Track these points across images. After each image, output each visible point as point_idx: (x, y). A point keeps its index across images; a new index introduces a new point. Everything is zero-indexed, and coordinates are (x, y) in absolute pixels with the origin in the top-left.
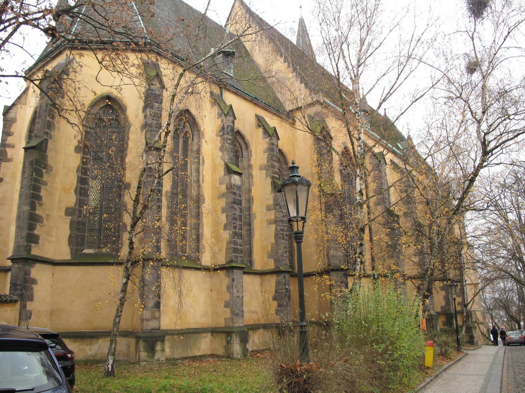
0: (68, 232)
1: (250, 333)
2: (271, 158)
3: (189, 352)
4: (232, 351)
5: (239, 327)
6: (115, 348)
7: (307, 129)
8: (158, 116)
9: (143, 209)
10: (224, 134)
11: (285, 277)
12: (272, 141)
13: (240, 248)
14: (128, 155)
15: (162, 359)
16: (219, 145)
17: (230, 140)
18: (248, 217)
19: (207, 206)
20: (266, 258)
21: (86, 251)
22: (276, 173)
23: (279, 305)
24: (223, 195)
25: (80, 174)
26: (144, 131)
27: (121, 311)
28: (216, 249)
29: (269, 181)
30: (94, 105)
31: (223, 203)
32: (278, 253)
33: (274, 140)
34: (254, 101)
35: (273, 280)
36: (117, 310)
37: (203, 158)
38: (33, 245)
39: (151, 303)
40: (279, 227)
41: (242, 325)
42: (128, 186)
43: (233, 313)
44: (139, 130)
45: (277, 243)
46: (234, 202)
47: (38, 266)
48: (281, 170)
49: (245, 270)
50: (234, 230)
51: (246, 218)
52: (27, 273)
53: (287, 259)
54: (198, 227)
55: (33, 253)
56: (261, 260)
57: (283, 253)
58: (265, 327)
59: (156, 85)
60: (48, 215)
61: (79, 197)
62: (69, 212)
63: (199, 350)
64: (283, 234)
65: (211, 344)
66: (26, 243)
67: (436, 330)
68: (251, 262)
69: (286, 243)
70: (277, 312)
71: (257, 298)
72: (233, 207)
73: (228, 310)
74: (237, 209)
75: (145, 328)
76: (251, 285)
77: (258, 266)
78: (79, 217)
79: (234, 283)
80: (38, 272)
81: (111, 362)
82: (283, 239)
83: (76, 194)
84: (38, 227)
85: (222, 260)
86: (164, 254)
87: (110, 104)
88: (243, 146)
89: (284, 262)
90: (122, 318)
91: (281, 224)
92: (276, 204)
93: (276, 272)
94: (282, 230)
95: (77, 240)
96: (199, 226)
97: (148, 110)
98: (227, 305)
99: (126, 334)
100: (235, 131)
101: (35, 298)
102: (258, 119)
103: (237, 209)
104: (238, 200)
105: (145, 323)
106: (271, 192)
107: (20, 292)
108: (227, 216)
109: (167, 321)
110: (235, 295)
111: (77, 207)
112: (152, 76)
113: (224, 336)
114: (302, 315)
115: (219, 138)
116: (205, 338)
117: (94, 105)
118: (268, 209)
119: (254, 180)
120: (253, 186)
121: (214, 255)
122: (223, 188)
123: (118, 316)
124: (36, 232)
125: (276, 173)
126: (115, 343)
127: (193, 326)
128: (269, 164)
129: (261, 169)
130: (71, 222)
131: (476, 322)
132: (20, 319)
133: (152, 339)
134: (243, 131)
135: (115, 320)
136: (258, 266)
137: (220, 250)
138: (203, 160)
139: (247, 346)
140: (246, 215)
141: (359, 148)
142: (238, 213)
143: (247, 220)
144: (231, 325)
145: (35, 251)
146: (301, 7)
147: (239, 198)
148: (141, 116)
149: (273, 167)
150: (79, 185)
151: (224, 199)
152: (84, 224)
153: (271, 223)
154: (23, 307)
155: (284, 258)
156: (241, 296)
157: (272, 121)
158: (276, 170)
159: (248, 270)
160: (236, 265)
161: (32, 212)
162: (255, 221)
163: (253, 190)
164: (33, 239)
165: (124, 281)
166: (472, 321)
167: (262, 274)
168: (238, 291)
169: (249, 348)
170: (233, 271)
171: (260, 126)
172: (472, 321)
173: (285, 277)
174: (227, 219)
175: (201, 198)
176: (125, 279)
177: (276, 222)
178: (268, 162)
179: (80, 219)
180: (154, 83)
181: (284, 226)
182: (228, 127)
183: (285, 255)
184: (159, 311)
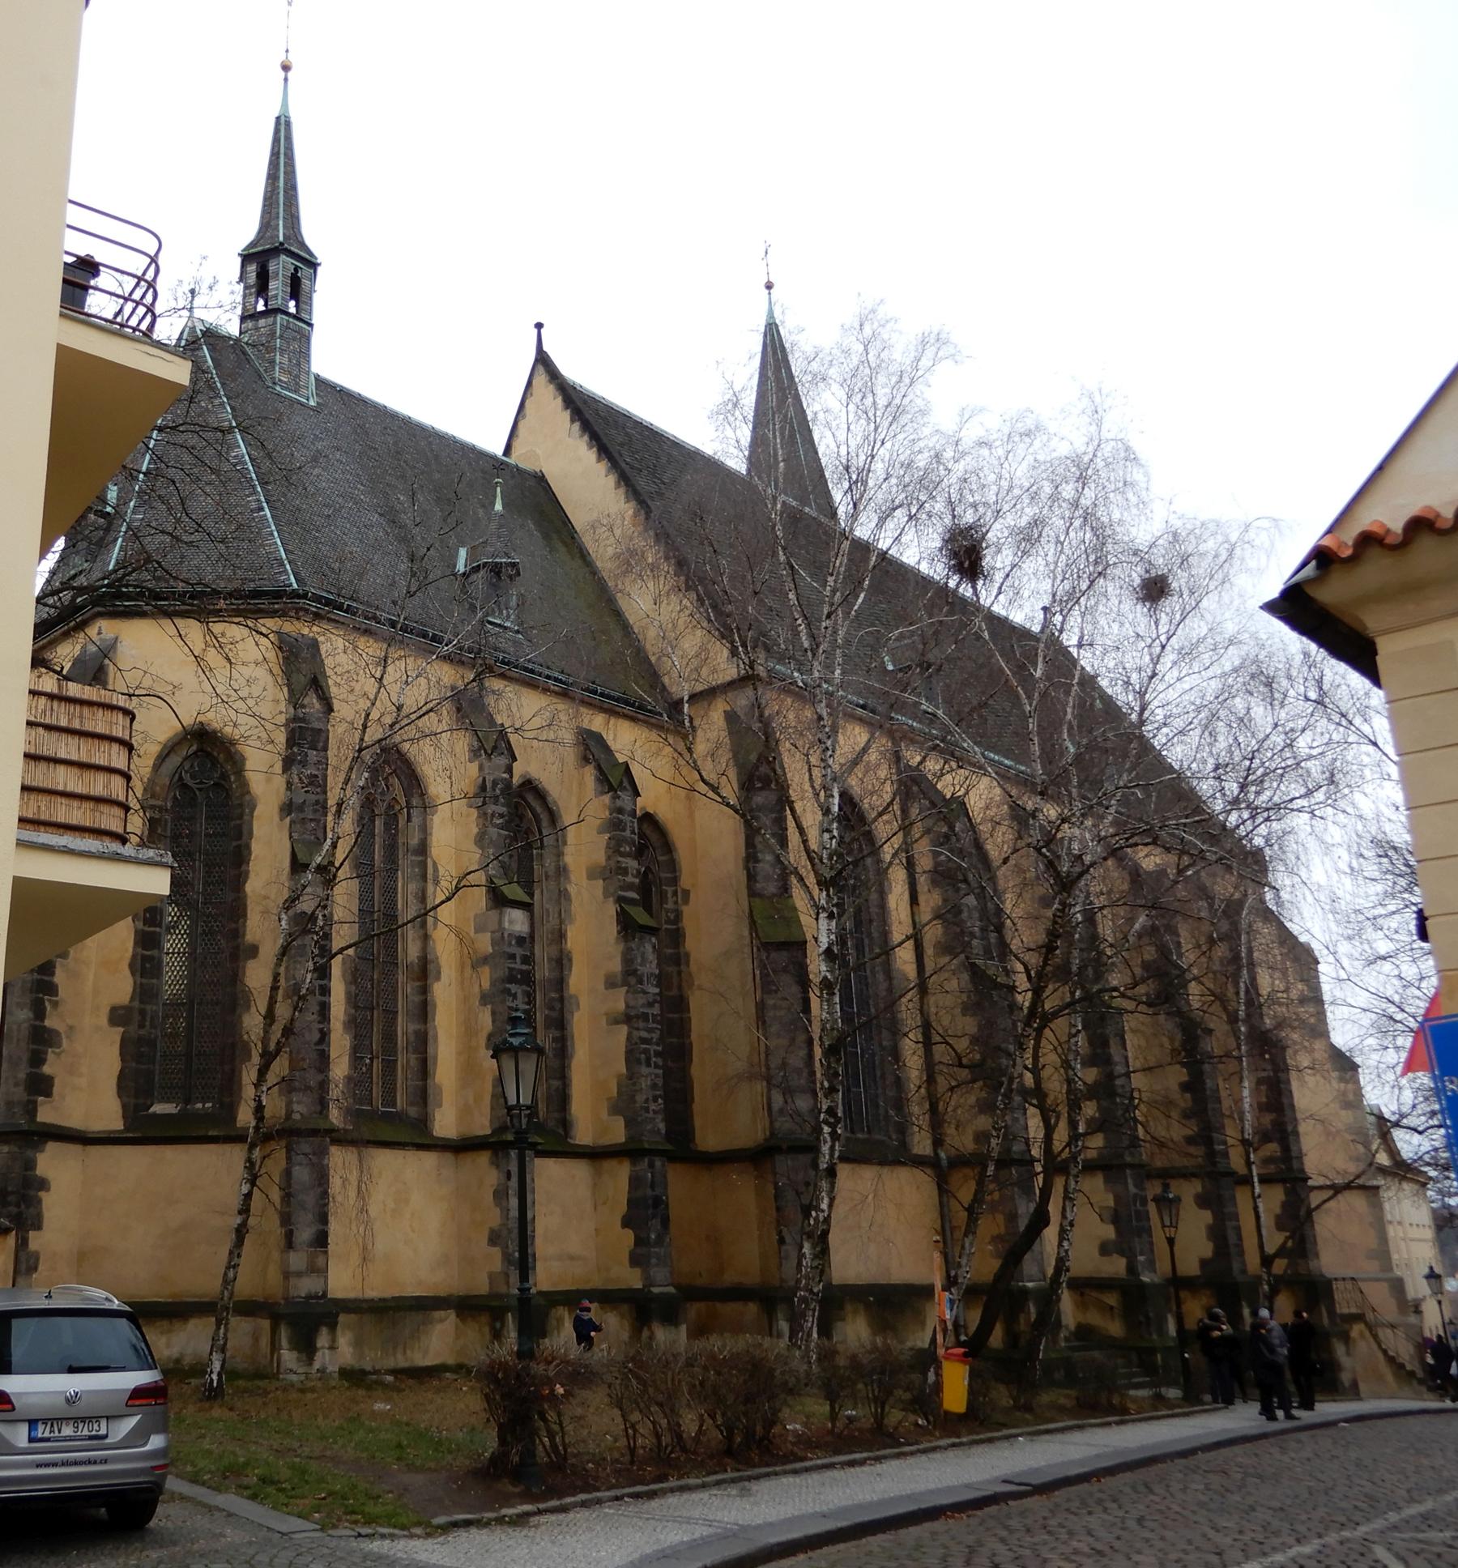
0: (117, 1066)
2: (614, 847)
3: (399, 1356)
6: (226, 1338)
8: (318, 783)
9: (283, 1035)
10: (484, 803)
11: (651, 1165)
12: (619, 803)
14: (252, 875)
15: (330, 1369)
16: (475, 830)
17: (501, 816)
18: (558, 1006)
19: (445, 993)
20: (604, 1115)
21: (158, 1108)
22: (630, 887)
23: (639, 1242)
24: (485, 960)
25: (140, 925)
27: (239, 1256)
29: (611, 909)
30: (167, 755)
32: (635, 1102)
33: (625, 798)
35: (620, 1174)
36: (231, 1253)
37: (435, 864)
38: (41, 1098)
39: (304, 1234)
40: (635, 1033)
42: (253, 951)
44: (277, 818)
45: (631, 1075)
46: (511, 979)
47: (51, 1146)
52: (30, 1165)
53: (660, 1117)
55: (39, 1119)
56: (591, 1117)
57: (647, 1101)
59: (313, 702)
60: (71, 1028)
61: (139, 980)
62: (118, 1016)
63: (426, 1352)
64: (646, 1051)
66: (25, 1097)
68: (566, 1124)
69: (657, 1076)
70: (635, 1260)
71: (576, 1223)
74: (519, 996)
76: (557, 1183)
78: (141, 1026)
80: (52, 1162)
81: (217, 1366)
82: (648, 1065)
83: (133, 974)
84: (50, 1056)
85: (482, 1126)
86: (335, 1117)
87: (205, 754)
89: (649, 1127)
90: (240, 1269)
91: (641, 1025)
92: (630, 975)
93: (627, 1152)
94: (644, 1041)
95: (135, 1085)
97: (295, 770)
99: (249, 1308)
101: (46, 1223)
103: (519, 996)
104: (521, 972)
105: (293, 1281)
107: (13, 1210)
108: (493, 1013)
109: (342, 1280)
111: (136, 1004)
112: (302, 673)
113: (484, 1319)
114: (524, 1263)
115: (474, 813)
116: (442, 1321)
117: (167, 755)
118: (610, 984)
119: (575, 907)
121: (465, 1112)
122: (485, 944)
123: (232, 1266)
124: (47, 1069)
125: (630, 887)
126: (226, 1325)
128: (612, 863)
130: (123, 1040)
132: (16, 1272)
133: (307, 1320)
135: (225, 1274)
136: (584, 1134)
141: (826, 836)
142: (520, 1003)
143: (555, 1014)
145: (46, 1114)
147: (525, 967)
148: (280, 782)
149: (624, 871)
150: (139, 950)
152: (152, 1043)
153: (617, 1022)
154: (22, 1243)
155: (651, 1115)
158: (630, 879)
160: (523, 1137)
161: (37, 1023)
162: (576, 1015)
163: (569, 934)
164: (41, 1086)
165: (245, 1189)
166: (1332, 1312)
167: (595, 1155)
170: (508, 1154)
173: (651, 1165)
174: (493, 1021)
175: (431, 967)
177: (628, 1018)
178: (609, 858)
179: (142, 1032)
180: (306, 702)
181: (650, 1030)
182: (495, 783)
183: (653, 1107)
184: (326, 1252)
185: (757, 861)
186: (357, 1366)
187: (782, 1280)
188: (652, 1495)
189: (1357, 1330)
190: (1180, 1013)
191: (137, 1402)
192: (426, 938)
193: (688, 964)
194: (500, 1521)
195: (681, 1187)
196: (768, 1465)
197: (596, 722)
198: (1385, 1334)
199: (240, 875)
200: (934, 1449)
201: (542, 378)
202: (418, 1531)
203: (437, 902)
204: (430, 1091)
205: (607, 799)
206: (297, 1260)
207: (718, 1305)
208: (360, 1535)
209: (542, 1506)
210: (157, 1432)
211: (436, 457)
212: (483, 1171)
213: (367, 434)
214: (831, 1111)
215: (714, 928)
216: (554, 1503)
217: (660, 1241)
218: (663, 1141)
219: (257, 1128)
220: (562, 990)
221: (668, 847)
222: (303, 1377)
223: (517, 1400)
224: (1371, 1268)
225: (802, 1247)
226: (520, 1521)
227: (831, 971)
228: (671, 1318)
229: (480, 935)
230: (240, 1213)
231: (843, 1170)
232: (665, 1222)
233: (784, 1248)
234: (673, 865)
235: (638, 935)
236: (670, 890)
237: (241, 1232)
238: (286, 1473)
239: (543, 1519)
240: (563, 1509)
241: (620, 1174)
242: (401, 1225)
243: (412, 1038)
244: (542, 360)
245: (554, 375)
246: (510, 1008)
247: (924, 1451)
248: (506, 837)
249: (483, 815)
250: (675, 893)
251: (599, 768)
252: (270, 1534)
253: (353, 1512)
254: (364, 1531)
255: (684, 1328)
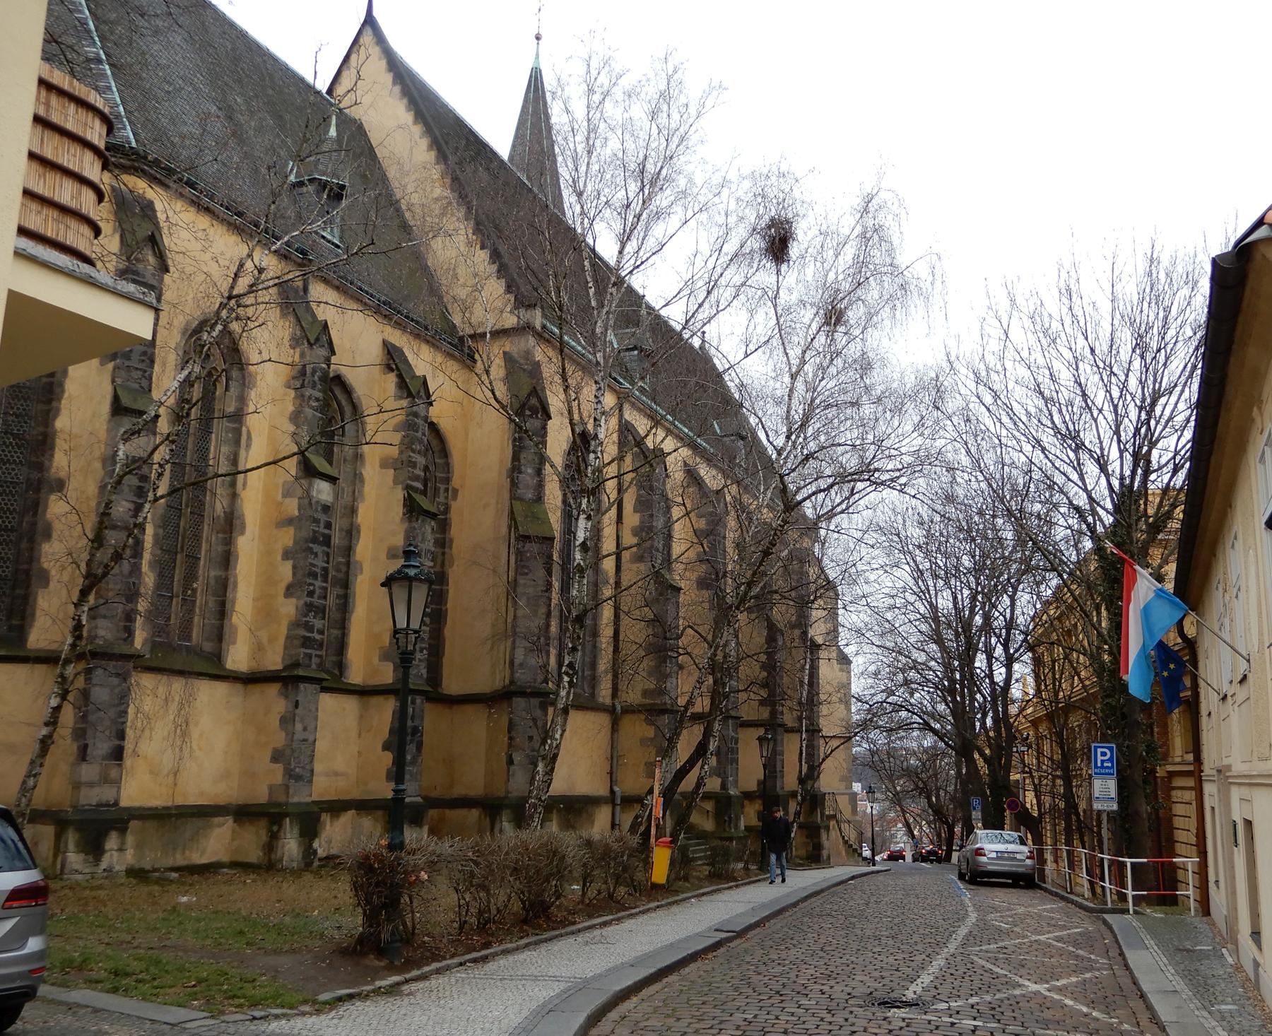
1: (325, 817)
2: (407, 445)
3: (178, 856)
4: (279, 853)
5: (299, 804)
7: (489, 394)
10: (302, 386)
13: (318, 637)
15: (117, 868)
16: (291, 408)
17: (317, 400)
18: (344, 569)
19: (247, 546)
20: (376, 660)
22: (416, 478)
24: (290, 522)
26: (111, 366)
27: (41, 765)
28: (264, 635)
29: (400, 494)
31: (287, 537)
34: (386, 310)
36: (32, 762)
39: (100, 747)
41: (308, 800)
43: (290, 774)
46: (314, 540)
48: (432, 468)
49: (325, 684)
50: (308, 599)
51: (338, 570)
53: (423, 665)
54: (223, 589)
56: (364, 658)
58: (363, 806)
63: (203, 853)
65: (233, 840)
67: (737, 827)
68: (341, 666)
71: (346, 745)
72: (310, 550)
73: (279, 768)
74: (320, 555)
75: (83, 801)
76: (335, 716)
77: (356, 675)
79: (297, 711)
85: (274, 661)
88: (348, 409)
96: (225, 587)
98: (277, 757)
100: (331, 375)
102: (389, 353)
103: (320, 555)
104: (324, 535)
105: (84, 791)
106: (402, 520)
108: (294, 567)
110: (296, 737)
113: (263, 823)
115: (292, 393)
116: (220, 826)
118: (392, 555)
119: (367, 489)
120: (363, 500)
121: (258, 648)
122: (292, 507)
125: (416, 478)
127: (193, 800)
128: (404, 457)
129: (384, 464)
131: (834, 817)
133: (97, 826)
134: (351, 376)
135: (24, 782)
136: (356, 675)
137: (272, 640)
138: (249, 437)
139: (316, 845)
140: (340, 563)
142: (320, 563)
143: (341, 576)
144: (282, 799)
146: (538, 38)
147: (326, 531)
149: (414, 465)
151: (291, 530)
156: (311, 739)
157: (422, 360)
159: (335, 683)
160: (311, 667)
162: (360, 578)
163: (360, 511)
165: (54, 702)
166: (822, 814)
167: (363, 692)
168: (305, 729)
169: (319, 851)
170: (297, 687)
171: (392, 370)
172: (822, 814)
174: (294, 574)
176: (58, 699)
178: (401, 452)
184: (120, 765)
185: (520, 472)
186: (137, 866)
187: (508, 792)
188: (485, 959)
189: (833, 823)
190: (768, 619)
191: (15, 904)
192: (234, 496)
193: (451, 548)
194: (378, 992)
195: (432, 720)
196: (553, 929)
197: (398, 338)
198: (845, 826)
199: (48, 412)
200: (648, 910)
201: (368, 38)
202: (307, 1008)
203: (249, 467)
204: (226, 630)
205: (405, 403)
206: (89, 771)
207: (447, 811)
208: (255, 1018)
209: (408, 976)
210: (34, 935)
211: (271, 76)
212: (272, 700)
213: (207, 31)
214: (571, 665)
215: (478, 518)
216: (415, 973)
217: (413, 762)
218: (417, 683)
219: (73, 646)
220: (349, 556)
221: (445, 453)
222: (88, 877)
223: (382, 886)
224: (841, 787)
225: (536, 766)
226: (393, 991)
227: (584, 560)
228: (417, 821)
229: (288, 500)
230: (46, 724)
231: (572, 713)
232: (419, 746)
233: (512, 768)
234: (447, 467)
235: (421, 518)
236: (442, 487)
237: (45, 744)
238: (136, 966)
239: (414, 986)
240: (424, 977)
241: (386, 710)
242: (186, 744)
243: (212, 582)
244: (369, 21)
245: (380, 39)
246: (312, 565)
247: (643, 912)
248: (321, 419)
249: (300, 397)
250: (447, 490)
251: (400, 376)
252: (156, 1026)
253: (234, 997)
254: (257, 1014)
255: (426, 828)
